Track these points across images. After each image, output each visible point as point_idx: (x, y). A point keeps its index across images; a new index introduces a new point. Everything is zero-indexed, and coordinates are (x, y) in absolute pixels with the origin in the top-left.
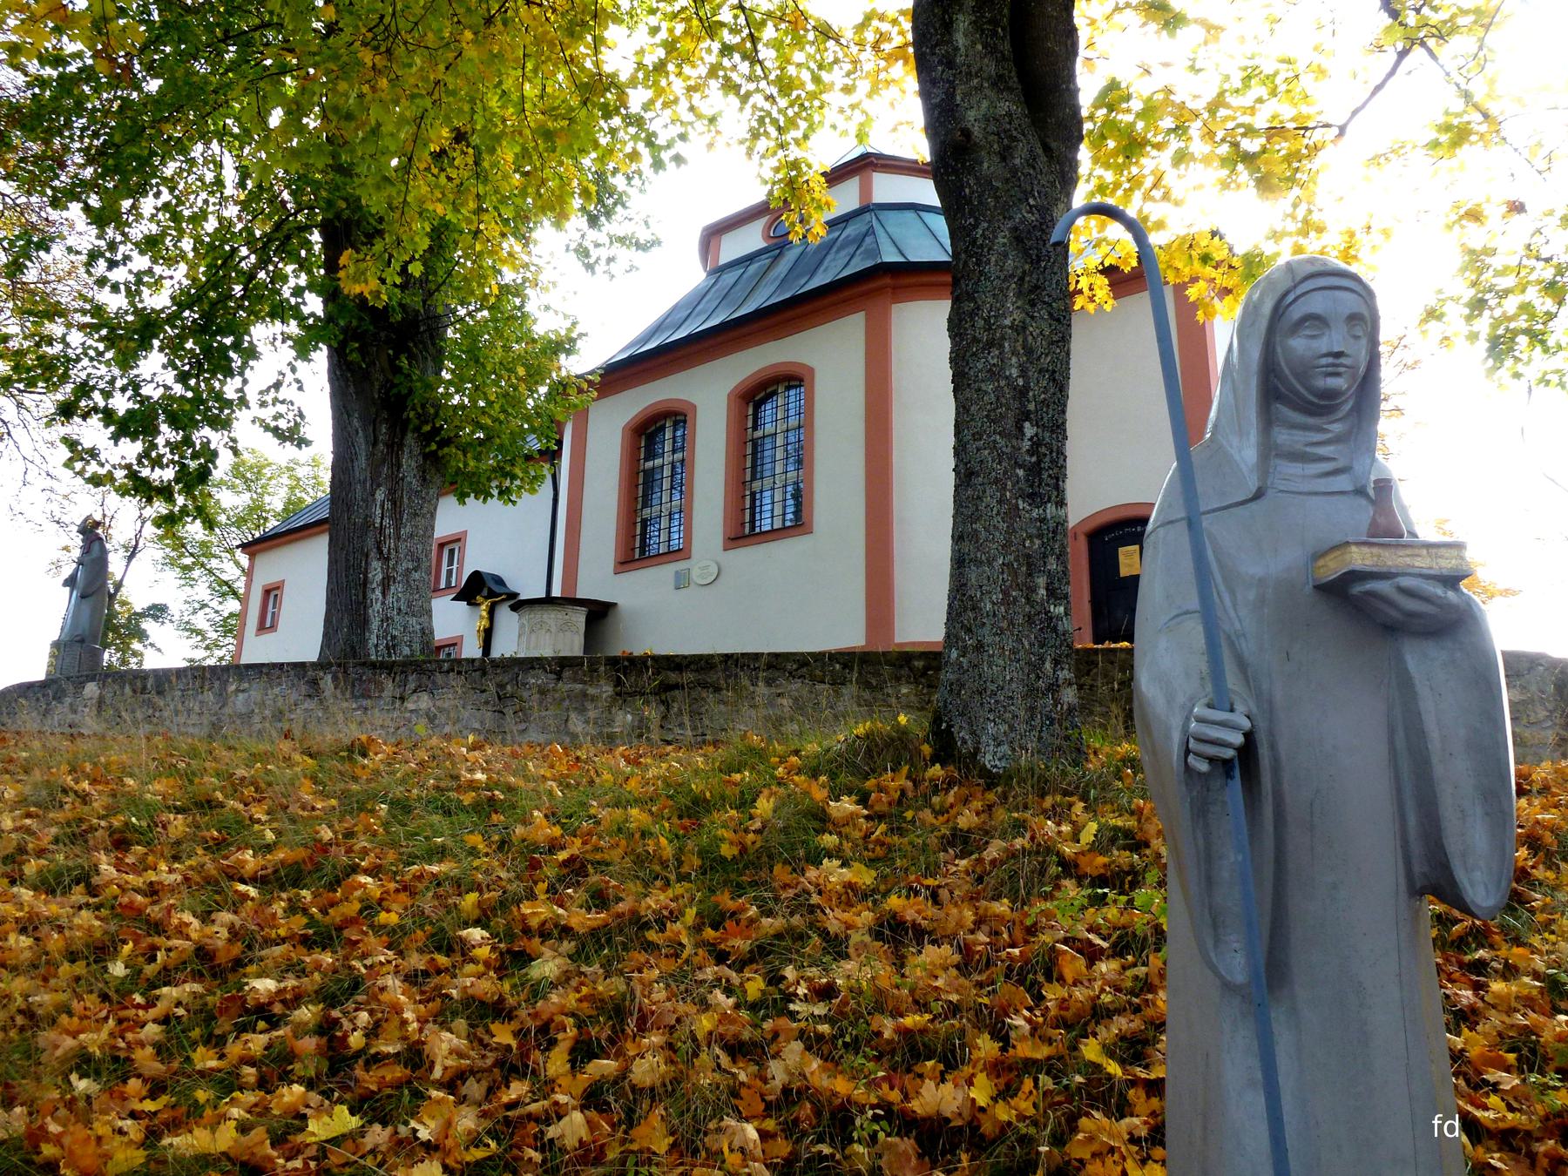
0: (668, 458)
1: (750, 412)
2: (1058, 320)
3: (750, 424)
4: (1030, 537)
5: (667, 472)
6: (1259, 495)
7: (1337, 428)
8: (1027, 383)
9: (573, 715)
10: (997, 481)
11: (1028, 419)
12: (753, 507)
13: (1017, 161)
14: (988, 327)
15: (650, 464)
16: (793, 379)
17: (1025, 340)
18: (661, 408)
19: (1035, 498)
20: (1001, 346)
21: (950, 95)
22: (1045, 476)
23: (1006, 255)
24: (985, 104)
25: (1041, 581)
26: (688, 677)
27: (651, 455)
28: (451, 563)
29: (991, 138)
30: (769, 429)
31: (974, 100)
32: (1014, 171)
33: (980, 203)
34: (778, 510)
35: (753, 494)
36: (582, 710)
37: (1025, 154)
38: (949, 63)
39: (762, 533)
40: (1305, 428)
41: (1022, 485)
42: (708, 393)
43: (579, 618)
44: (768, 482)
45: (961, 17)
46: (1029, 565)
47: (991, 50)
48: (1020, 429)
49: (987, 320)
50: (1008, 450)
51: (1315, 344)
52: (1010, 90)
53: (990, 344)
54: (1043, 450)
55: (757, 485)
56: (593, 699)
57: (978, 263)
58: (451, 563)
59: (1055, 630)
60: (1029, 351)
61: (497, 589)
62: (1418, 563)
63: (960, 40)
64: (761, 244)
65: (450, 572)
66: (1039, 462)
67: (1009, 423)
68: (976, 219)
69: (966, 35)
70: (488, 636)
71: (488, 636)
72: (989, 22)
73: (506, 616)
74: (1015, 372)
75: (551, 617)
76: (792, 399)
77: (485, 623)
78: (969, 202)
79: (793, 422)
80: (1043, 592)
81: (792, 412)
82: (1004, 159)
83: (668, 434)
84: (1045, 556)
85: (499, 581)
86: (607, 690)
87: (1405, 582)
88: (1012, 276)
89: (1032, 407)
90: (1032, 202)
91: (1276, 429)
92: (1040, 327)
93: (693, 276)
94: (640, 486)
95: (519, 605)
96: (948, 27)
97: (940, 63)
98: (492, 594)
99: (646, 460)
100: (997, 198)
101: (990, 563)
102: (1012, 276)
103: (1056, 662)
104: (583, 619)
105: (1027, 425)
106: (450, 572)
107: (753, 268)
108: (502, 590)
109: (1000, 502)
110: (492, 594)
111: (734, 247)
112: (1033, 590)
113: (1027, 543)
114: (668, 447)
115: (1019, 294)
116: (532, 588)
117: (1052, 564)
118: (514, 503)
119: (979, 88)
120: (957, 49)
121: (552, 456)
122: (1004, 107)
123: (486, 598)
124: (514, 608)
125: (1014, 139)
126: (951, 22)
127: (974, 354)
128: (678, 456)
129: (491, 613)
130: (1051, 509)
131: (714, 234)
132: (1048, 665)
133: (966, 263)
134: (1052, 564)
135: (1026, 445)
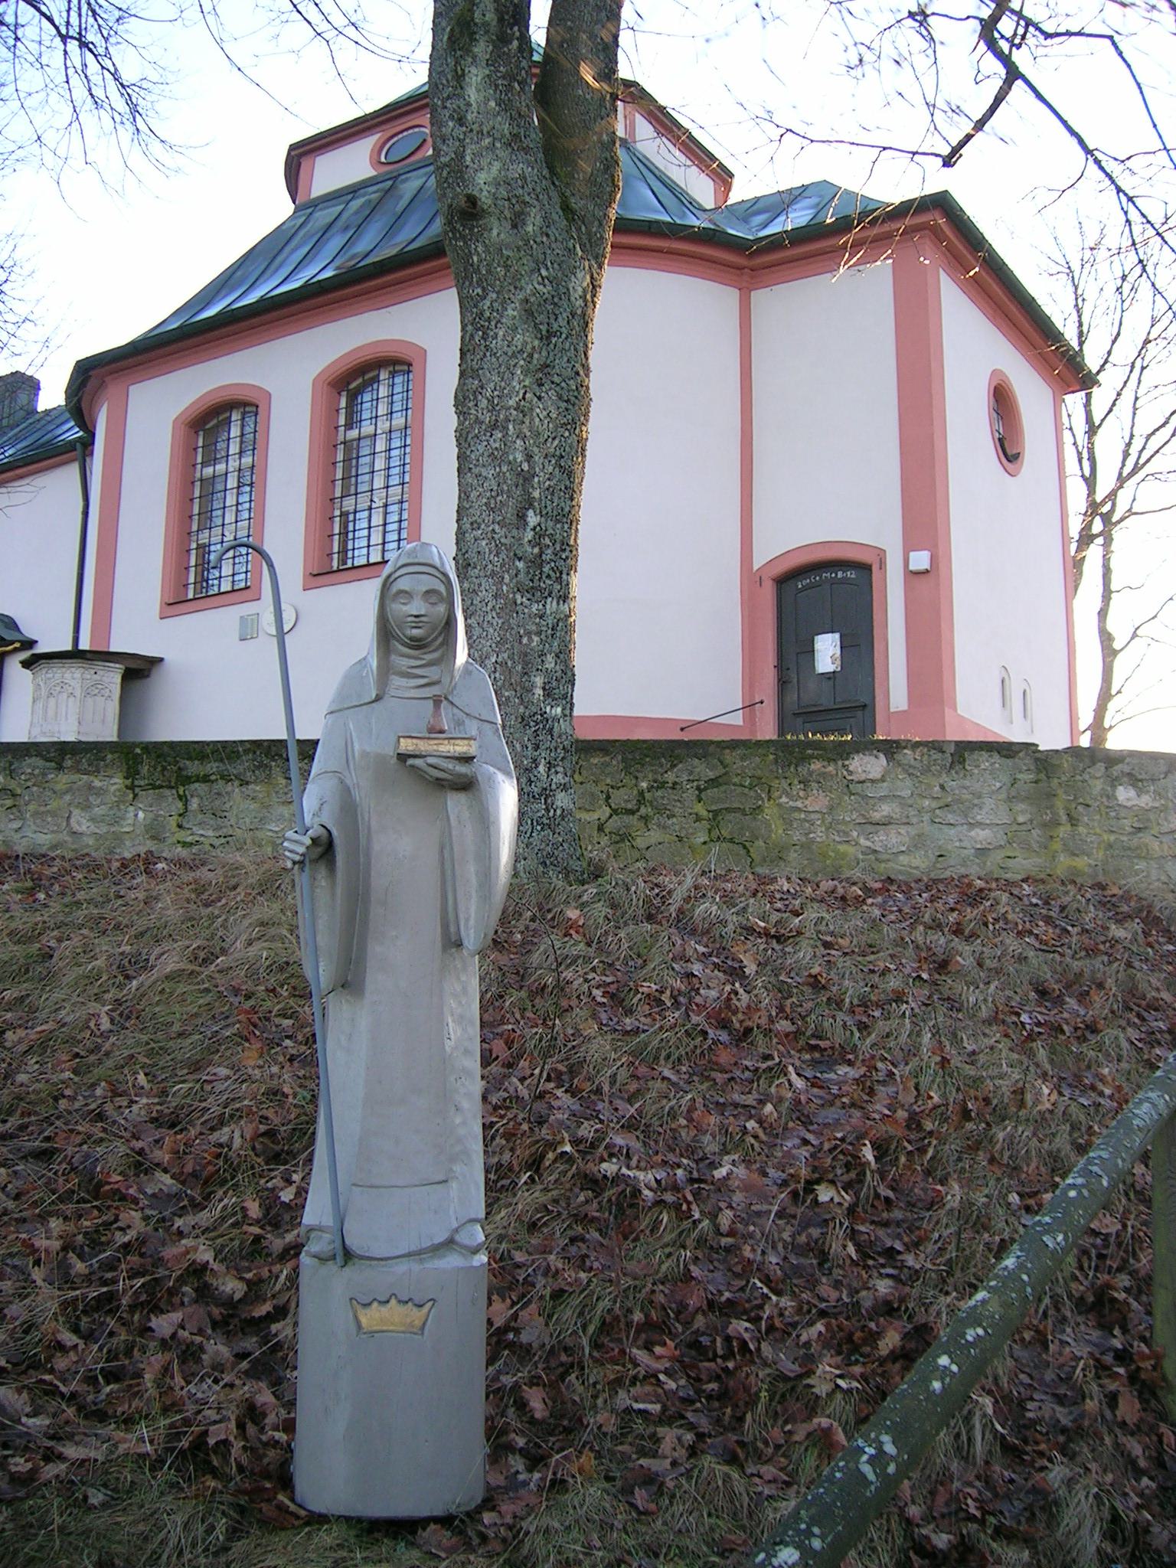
0: (233, 464)
1: (343, 403)
3: (342, 421)
4: (529, 634)
5: (232, 482)
7: (436, 655)
9: (76, 812)
11: (531, 506)
12: (344, 533)
13: (530, 229)
14: (492, 408)
15: (209, 471)
16: (394, 364)
18: (226, 396)
19: (533, 591)
22: (546, 569)
23: (515, 329)
24: (497, 165)
26: (212, 767)
27: (211, 460)
30: (367, 429)
31: (484, 162)
33: (489, 272)
34: (377, 538)
35: (344, 515)
36: (86, 807)
37: (539, 221)
38: (461, 121)
39: (354, 568)
42: (286, 374)
43: (113, 677)
44: (363, 502)
45: (474, 70)
46: (526, 664)
47: (505, 105)
48: (522, 517)
49: (490, 401)
51: (405, 608)
52: (526, 150)
53: (494, 426)
55: (349, 504)
56: (100, 792)
57: (484, 338)
62: (442, 748)
63: (473, 94)
64: (369, 172)
67: (510, 513)
68: (484, 289)
69: (478, 91)
72: (504, 77)
74: (520, 457)
75: (73, 675)
76: (398, 389)
78: (478, 271)
79: (399, 421)
81: (397, 407)
82: (514, 226)
83: (235, 431)
84: (542, 654)
86: (118, 781)
87: (430, 760)
88: (521, 351)
90: (544, 273)
91: (393, 657)
92: (545, 411)
93: (276, 208)
94: (195, 501)
97: (451, 117)
99: (204, 464)
100: (507, 267)
103: (550, 766)
104: (118, 679)
105: (531, 513)
107: (356, 204)
108: (18, 637)
111: (335, 172)
113: (525, 640)
114: (234, 448)
115: (526, 372)
116: (54, 638)
117: (550, 662)
120: (469, 104)
122: (517, 169)
124: (27, 664)
125: (525, 203)
126: (463, 75)
130: (551, 605)
131: (300, 157)
132: (542, 768)
133: (472, 335)
134: (550, 662)
135: (529, 535)
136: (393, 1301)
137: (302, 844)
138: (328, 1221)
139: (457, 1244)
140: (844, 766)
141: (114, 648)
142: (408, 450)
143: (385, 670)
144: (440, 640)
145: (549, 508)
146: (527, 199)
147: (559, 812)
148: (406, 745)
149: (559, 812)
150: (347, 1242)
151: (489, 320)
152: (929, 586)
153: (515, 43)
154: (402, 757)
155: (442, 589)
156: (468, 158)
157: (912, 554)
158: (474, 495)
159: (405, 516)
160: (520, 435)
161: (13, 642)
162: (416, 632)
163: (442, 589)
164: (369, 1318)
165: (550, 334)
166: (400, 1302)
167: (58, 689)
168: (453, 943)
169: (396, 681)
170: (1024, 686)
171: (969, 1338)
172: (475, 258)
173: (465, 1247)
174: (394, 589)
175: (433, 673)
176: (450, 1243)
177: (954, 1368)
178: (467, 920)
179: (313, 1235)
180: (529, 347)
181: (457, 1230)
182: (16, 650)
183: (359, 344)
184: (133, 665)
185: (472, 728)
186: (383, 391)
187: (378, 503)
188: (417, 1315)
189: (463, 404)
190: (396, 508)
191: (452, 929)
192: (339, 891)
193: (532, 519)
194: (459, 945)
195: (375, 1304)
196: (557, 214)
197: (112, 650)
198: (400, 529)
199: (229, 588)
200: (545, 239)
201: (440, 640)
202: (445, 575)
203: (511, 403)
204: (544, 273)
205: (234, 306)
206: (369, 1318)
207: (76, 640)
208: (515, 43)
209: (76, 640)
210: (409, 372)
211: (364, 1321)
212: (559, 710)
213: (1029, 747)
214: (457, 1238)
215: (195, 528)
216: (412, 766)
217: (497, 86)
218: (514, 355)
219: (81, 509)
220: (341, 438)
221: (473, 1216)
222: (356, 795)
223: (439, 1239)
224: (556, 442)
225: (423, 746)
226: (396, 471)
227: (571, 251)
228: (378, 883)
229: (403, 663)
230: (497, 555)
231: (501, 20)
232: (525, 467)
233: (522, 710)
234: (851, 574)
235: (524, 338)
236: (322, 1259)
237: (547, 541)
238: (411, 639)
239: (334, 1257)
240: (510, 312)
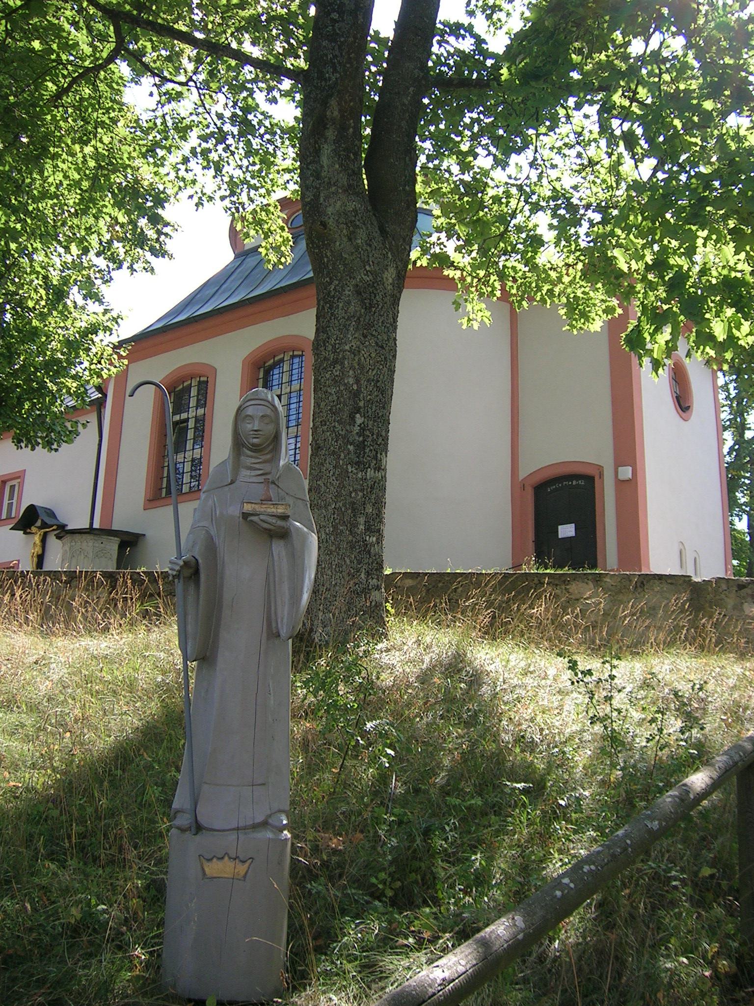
1: (261, 375)
2: (382, 347)
4: (355, 491)
6: (232, 482)
7: (268, 456)
8: (359, 388)
10: (334, 453)
11: (358, 412)
13: (359, 241)
17: (360, 359)
19: (361, 465)
20: (342, 364)
21: (317, 197)
22: (367, 450)
23: (349, 303)
24: (339, 203)
25: (362, 520)
28: (11, 497)
29: (342, 226)
31: (332, 201)
32: (357, 248)
37: (364, 237)
38: (318, 177)
40: (252, 457)
41: (352, 456)
43: (113, 546)
45: (326, 146)
46: (354, 510)
49: (334, 346)
50: (343, 433)
53: (336, 362)
54: (368, 433)
57: (331, 308)
58: (11, 497)
59: (369, 552)
60: (362, 367)
61: (48, 521)
63: (325, 161)
65: (10, 505)
66: (364, 441)
67: (345, 416)
68: (331, 279)
70: (40, 560)
71: (40, 560)
72: (344, 151)
73: (53, 543)
74: (351, 381)
75: (88, 544)
77: (38, 550)
79: (295, 386)
80: (362, 527)
81: (295, 377)
82: (350, 239)
85: (51, 514)
87: (262, 517)
88: (354, 316)
89: (361, 404)
90: (368, 268)
91: (242, 457)
95: (63, 532)
96: (317, 152)
98: (44, 525)
100: (345, 265)
101: (326, 507)
102: (354, 316)
104: (116, 547)
105: (358, 416)
106: (10, 505)
109: (335, 467)
110: (44, 525)
112: (356, 525)
113: (353, 495)
114: (193, 402)
115: (357, 329)
117: (369, 509)
118: (56, 450)
119: (336, 193)
120: (322, 167)
121: (99, 404)
122: (351, 206)
123: (40, 528)
124: (59, 537)
125: (357, 227)
126: (320, 150)
127: (325, 368)
128: (201, 411)
129: (44, 541)
130: (370, 473)
134: (369, 509)
135: (357, 429)
136: (226, 858)
137: (177, 564)
138: (188, 806)
139: (270, 825)
140: (566, 589)
142: (301, 404)
143: (237, 465)
144: (271, 447)
145: (370, 413)
146: (358, 223)
147: (373, 604)
148: (248, 508)
149: (373, 604)
150: (199, 818)
151: (333, 297)
152: (630, 493)
153: (351, 130)
154: (245, 516)
155: (269, 412)
156: (322, 199)
157: (620, 468)
158: (323, 404)
159: (299, 445)
160: (352, 367)
162: (255, 441)
163: (272, 414)
164: (212, 869)
165: (371, 306)
166: (230, 858)
168: (273, 635)
169: (244, 473)
170: (695, 555)
171: (585, 870)
172: (326, 260)
173: (273, 827)
174: (243, 415)
175: (267, 467)
176: (265, 824)
177: (572, 885)
178: (282, 618)
179: (179, 815)
180: (358, 314)
181: (270, 816)
182: (54, 530)
183: (176, 367)
184: (126, 538)
185: (290, 501)
186: (286, 367)
188: (242, 869)
189: (317, 349)
191: (274, 625)
192: (202, 597)
193: (359, 419)
194: (278, 635)
195: (215, 860)
196: (377, 234)
197: (113, 528)
198: (295, 454)
200: (368, 248)
201: (271, 447)
202: (274, 406)
203: (347, 347)
204: (368, 268)
206: (212, 869)
207: (92, 523)
208: (351, 130)
209: (92, 523)
210: (302, 355)
211: (206, 869)
212: (374, 539)
213: (685, 580)
214: (270, 821)
216: (252, 521)
217: (340, 156)
218: (349, 319)
221: (282, 808)
222: (216, 540)
223: (259, 819)
224: (375, 372)
225: (258, 508)
226: (294, 417)
227: (385, 256)
228: (227, 597)
229: (249, 461)
230: (336, 441)
231: (342, 116)
232: (355, 387)
233: (350, 538)
234: (582, 482)
235: (354, 307)
236: (183, 830)
237: (368, 433)
238: (253, 445)
239: (189, 829)
240: (347, 292)
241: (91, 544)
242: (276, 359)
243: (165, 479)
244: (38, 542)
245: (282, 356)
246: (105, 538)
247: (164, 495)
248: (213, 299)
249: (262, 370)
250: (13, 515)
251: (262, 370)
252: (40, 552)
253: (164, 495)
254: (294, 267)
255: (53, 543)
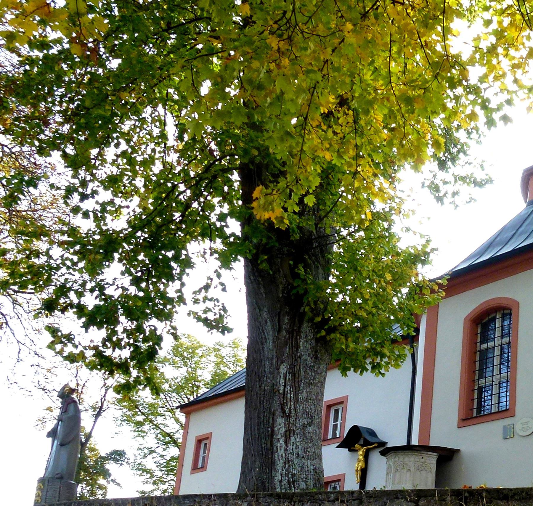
0: (498, 342)
5: (497, 352)
15: (484, 346)
18: (493, 304)
28: (336, 420)
39: (484, 415)
43: (432, 460)
58: (336, 420)
61: (370, 439)
65: (335, 427)
70: (364, 474)
71: (364, 474)
75: (411, 460)
77: (361, 464)
83: (498, 324)
85: (372, 433)
95: (387, 451)
98: (367, 443)
99: (482, 342)
106: (335, 427)
114: (498, 333)
116: (396, 438)
123: (363, 446)
124: (383, 453)
128: (506, 340)
141: (433, 443)
161: (373, 443)
167: (401, 467)
182: (375, 447)
183: (485, 300)
187: (496, 382)
190: (505, 385)
199: (497, 410)
205: (497, 254)
215: (477, 378)
219: (411, 370)
220: (478, 349)
241: (412, 459)
242: (490, 317)
243: (476, 401)
244: (361, 457)
245: (494, 315)
246: (424, 454)
247: (475, 415)
248: (512, 241)
249: (480, 326)
250: (338, 436)
251: (480, 326)
252: (363, 466)
253: (475, 415)
254: (237, 375)
255: (376, 458)
